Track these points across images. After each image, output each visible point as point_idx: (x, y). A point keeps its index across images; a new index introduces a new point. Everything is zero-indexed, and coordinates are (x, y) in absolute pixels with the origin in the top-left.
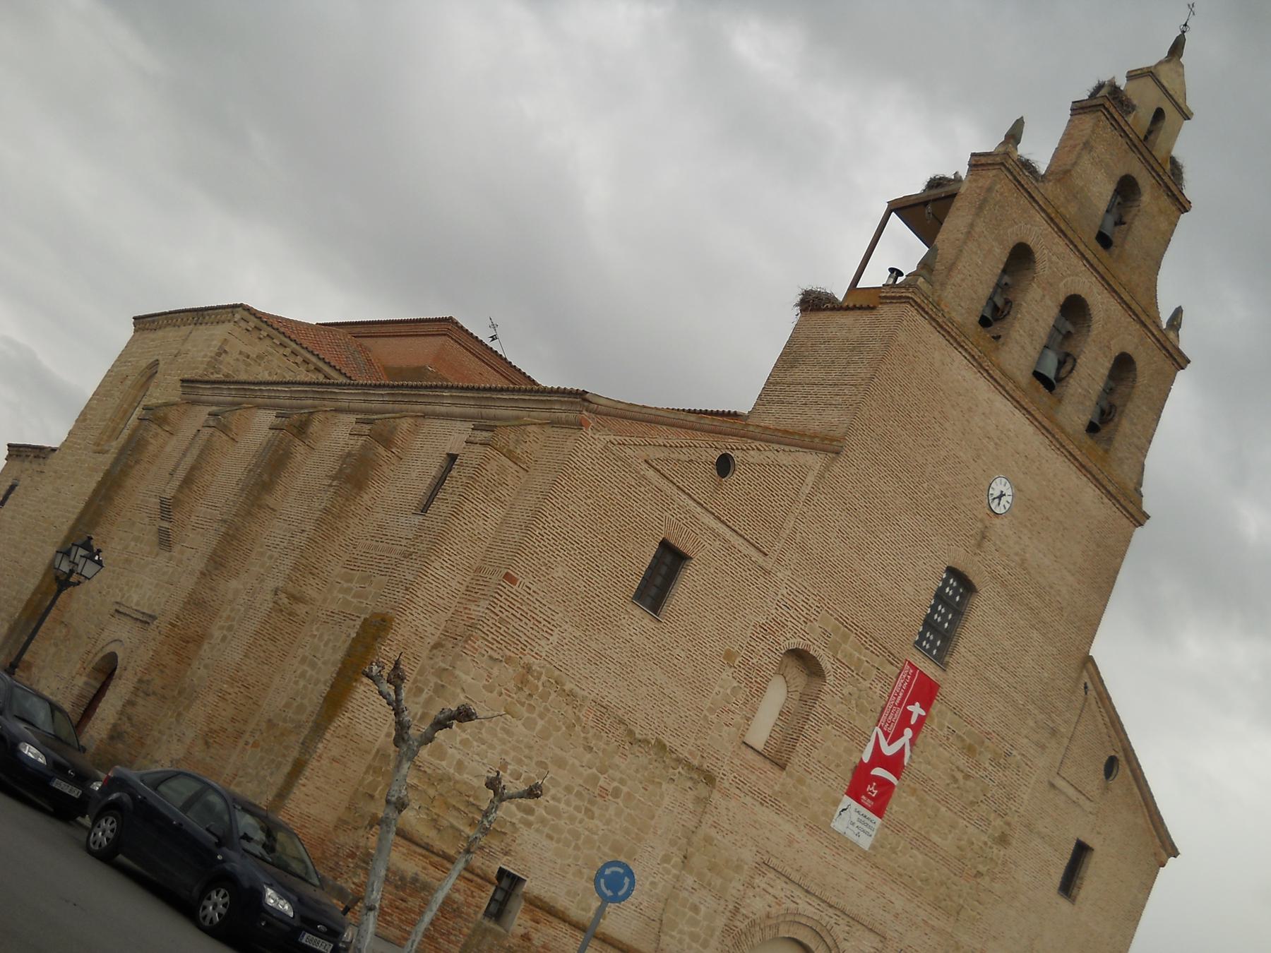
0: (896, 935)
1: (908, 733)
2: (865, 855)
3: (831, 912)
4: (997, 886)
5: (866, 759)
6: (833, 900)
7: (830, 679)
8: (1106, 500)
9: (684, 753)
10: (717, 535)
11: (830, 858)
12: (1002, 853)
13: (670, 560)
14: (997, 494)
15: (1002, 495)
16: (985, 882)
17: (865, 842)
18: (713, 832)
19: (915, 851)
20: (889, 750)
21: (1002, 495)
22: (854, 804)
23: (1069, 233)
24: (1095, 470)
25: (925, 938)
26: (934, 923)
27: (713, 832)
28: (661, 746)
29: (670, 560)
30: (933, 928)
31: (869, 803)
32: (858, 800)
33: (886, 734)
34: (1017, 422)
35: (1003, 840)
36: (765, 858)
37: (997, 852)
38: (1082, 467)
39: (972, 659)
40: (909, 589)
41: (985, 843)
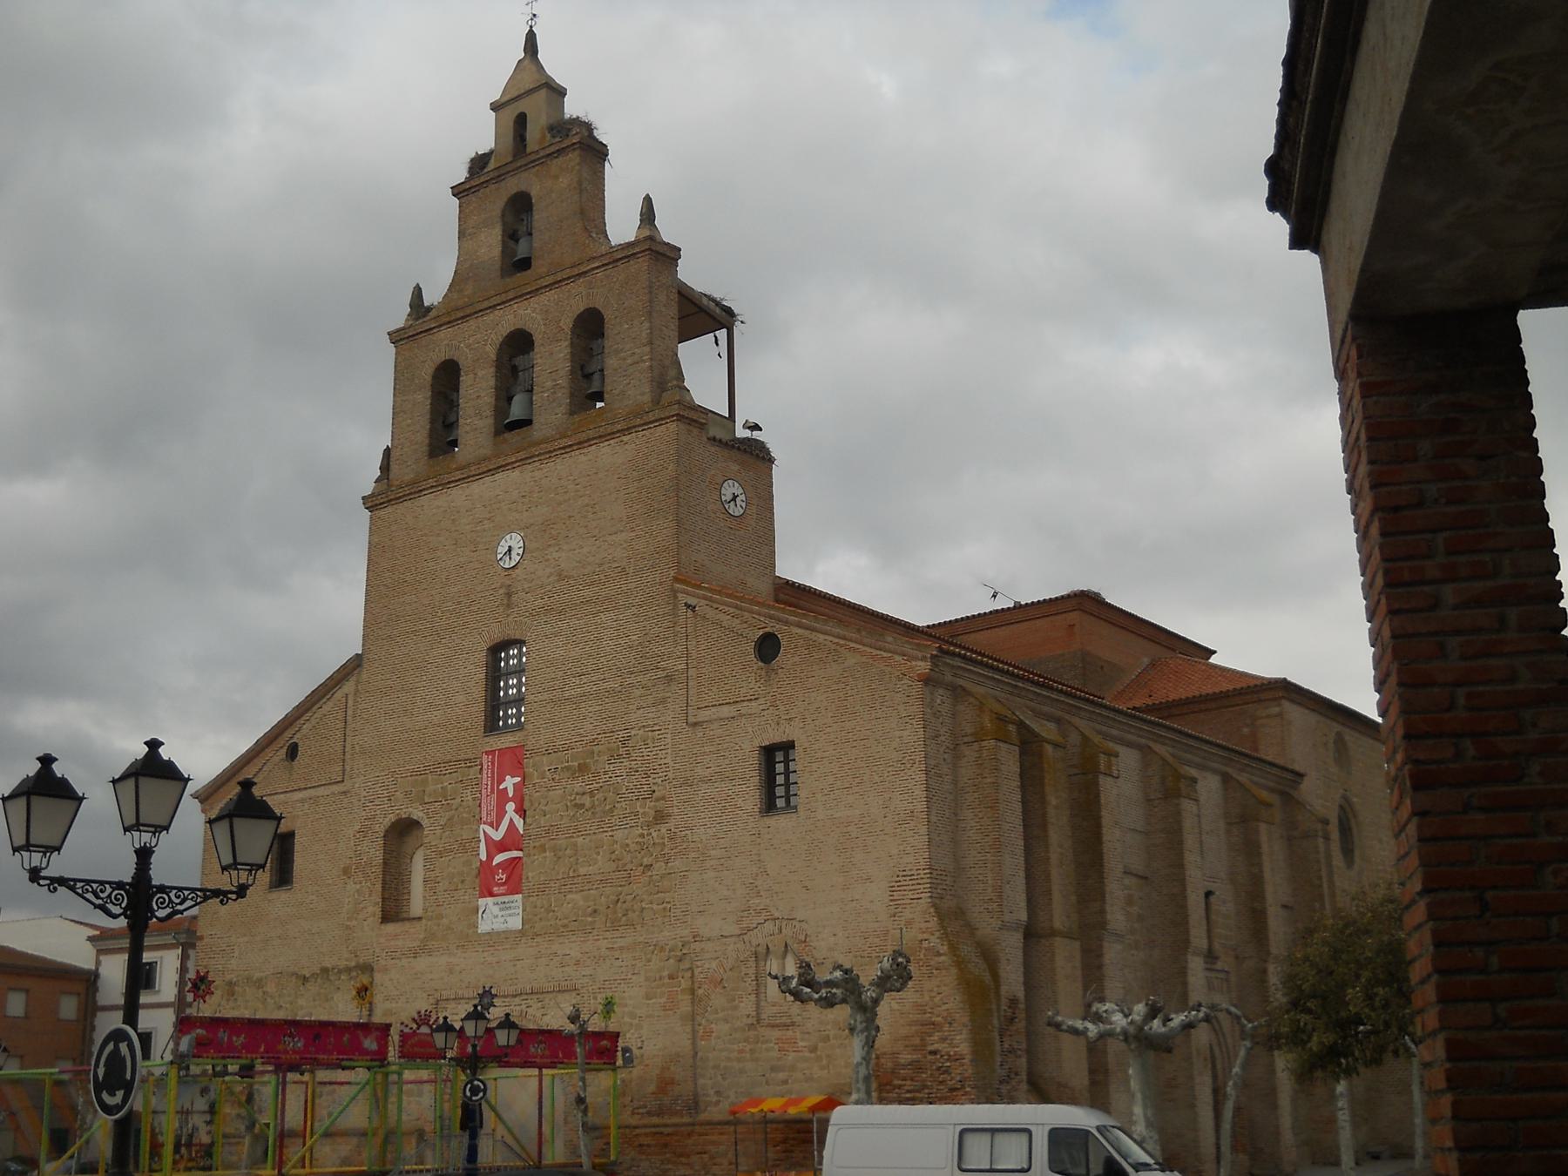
0: (586, 980)
1: (510, 807)
2: (522, 933)
3: (517, 1000)
4: (677, 864)
5: (483, 857)
6: (511, 990)
7: (425, 823)
8: (625, 438)
9: (342, 964)
10: (302, 801)
11: (490, 959)
12: (664, 830)
13: (775, 756)
14: (729, 497)
15: (735, 497)
16: (659, 868)
17: (516, 923)
18: (388, 1005)
19: (570, 896)
20: (498, 835)
21: (735, 497)
22: (490, 900)
23: (468, 311)
24: (591, 434)
25: (619, 963)
26: (621, 943)
27: (388, 1005)
28: (325, 970)
29: (775, 756)
30: (621, 948)
31: (503, 889)
32: (491, 895)
33: (491, 825)
34: (459, 496)
35: (660, 817)
36: (437, 995)
37: (659, 833)
38: (581, 444)
39: (545, 696)
40: (461, 698)
41: (642, 836)
